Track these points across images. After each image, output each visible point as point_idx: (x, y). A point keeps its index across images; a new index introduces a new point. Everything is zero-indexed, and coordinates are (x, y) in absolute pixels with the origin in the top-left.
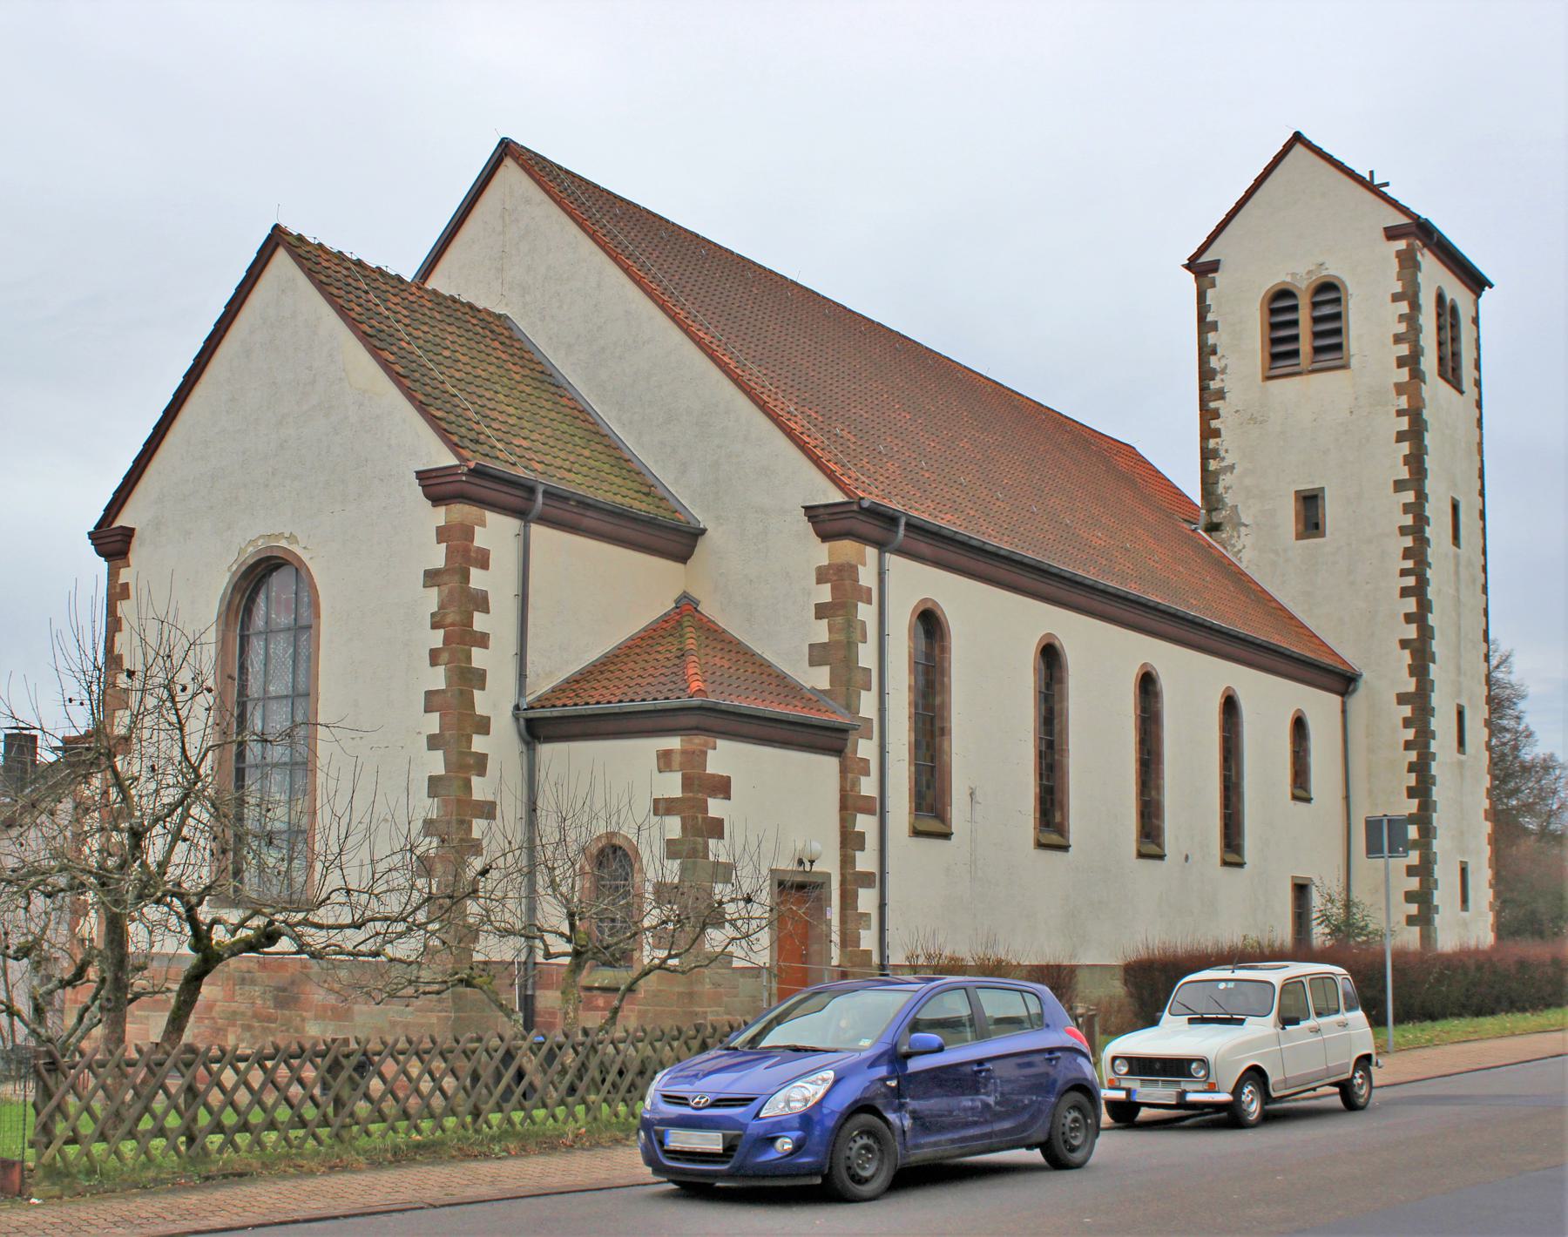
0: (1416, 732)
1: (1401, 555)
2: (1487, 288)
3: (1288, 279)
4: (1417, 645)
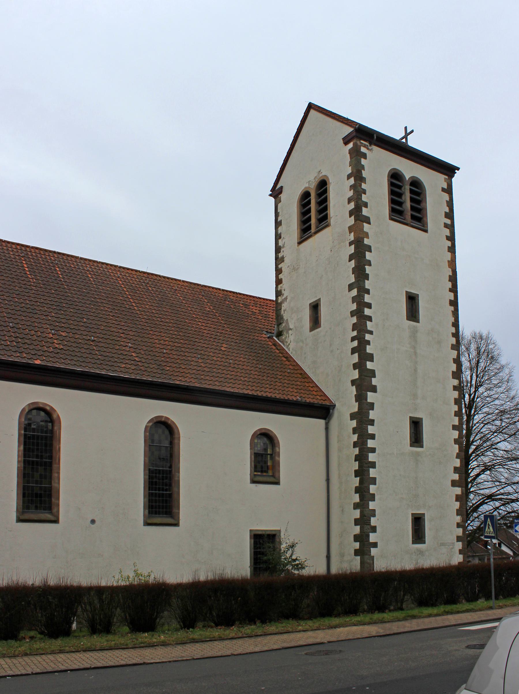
0: (358, 436)
1: (371, 335)
2: (456, 171)
3: (307, 186)
4: (358, 381)
